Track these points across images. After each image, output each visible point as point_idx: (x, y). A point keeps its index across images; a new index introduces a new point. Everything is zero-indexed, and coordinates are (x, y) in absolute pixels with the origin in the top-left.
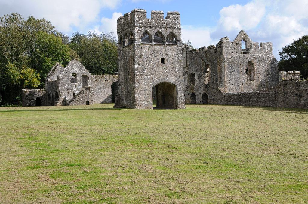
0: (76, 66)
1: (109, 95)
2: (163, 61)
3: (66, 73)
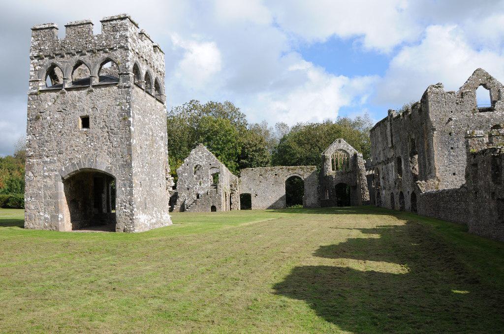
0: (201, 155)
1: (281, 196)
2: (86, 122)
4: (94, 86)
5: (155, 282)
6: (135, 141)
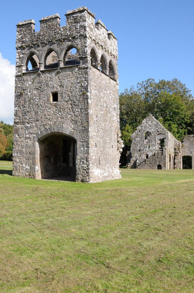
0: (151, 124)
2: (55, 96)
4: (61, 68)
5: (89, 225)
6: (91, 111)
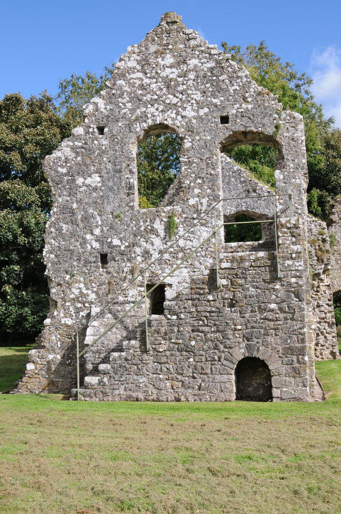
0: (172, 73)
3: (101, 130)
